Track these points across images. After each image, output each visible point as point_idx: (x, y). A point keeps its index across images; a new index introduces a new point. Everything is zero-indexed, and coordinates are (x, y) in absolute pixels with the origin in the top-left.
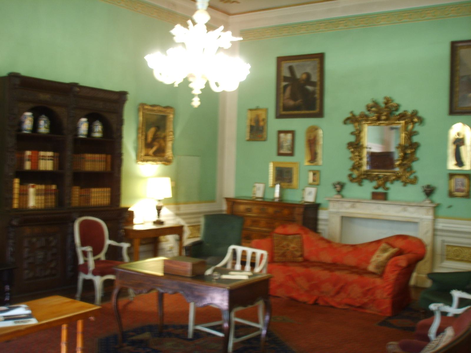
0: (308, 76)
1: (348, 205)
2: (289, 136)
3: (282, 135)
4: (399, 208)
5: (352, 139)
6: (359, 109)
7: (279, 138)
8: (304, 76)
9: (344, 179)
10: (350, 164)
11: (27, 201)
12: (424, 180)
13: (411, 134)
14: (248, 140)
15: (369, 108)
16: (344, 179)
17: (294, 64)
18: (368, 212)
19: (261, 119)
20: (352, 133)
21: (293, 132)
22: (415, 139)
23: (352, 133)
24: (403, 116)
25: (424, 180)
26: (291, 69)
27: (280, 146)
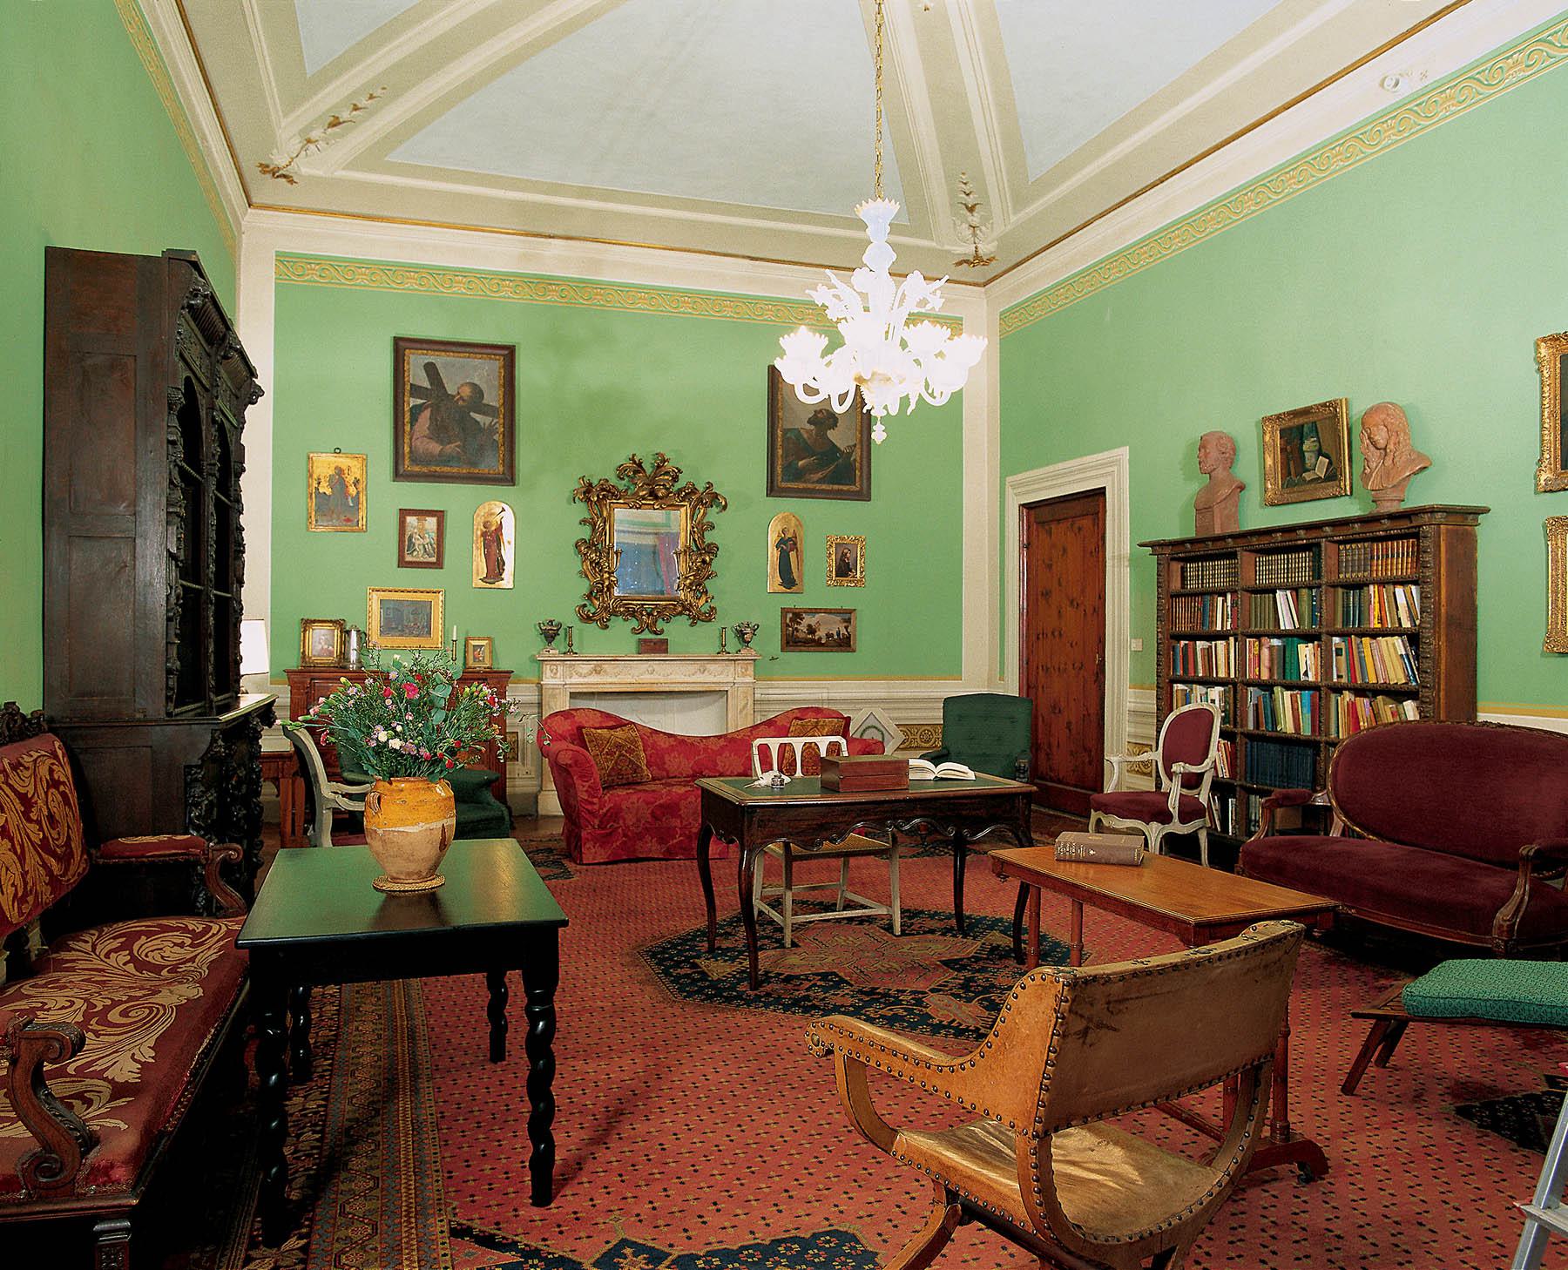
0: (478, 392)
1: (585, 668)
2: (431, 522)
3: (411, 520)
4: (693, 667)
5: (585, 533)
6: (603, 470)
7: (402, 524)
8: (466, 392)
9: (569, 618)
10: (584, 586)
11: (1356, 682)
12: (730, 617)
13: (701, 528)
14: (1486, 511)
15: (621, 472)
16: (569, 618)
17: (439, 360)
18: (647, 678)
19: (350, 479)
20: (584, 522)
21: (440, 515)
22: (710, 537)
23: (584, 522)
24: (689, 493)
25: (730, 617)
26: (431, 369)
27: (404, 542)
